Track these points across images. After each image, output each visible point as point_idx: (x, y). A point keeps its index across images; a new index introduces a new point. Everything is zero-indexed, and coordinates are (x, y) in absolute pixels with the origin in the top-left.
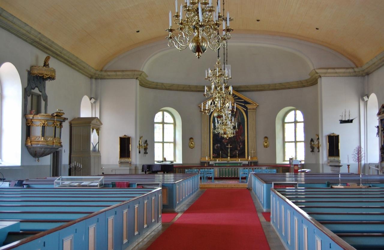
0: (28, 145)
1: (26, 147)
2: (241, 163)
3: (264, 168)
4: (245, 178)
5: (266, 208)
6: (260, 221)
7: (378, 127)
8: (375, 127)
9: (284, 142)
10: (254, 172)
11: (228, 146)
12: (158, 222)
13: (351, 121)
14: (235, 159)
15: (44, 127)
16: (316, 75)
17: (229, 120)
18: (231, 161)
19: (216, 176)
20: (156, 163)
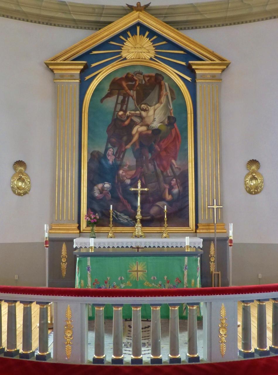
11: (137, 187)
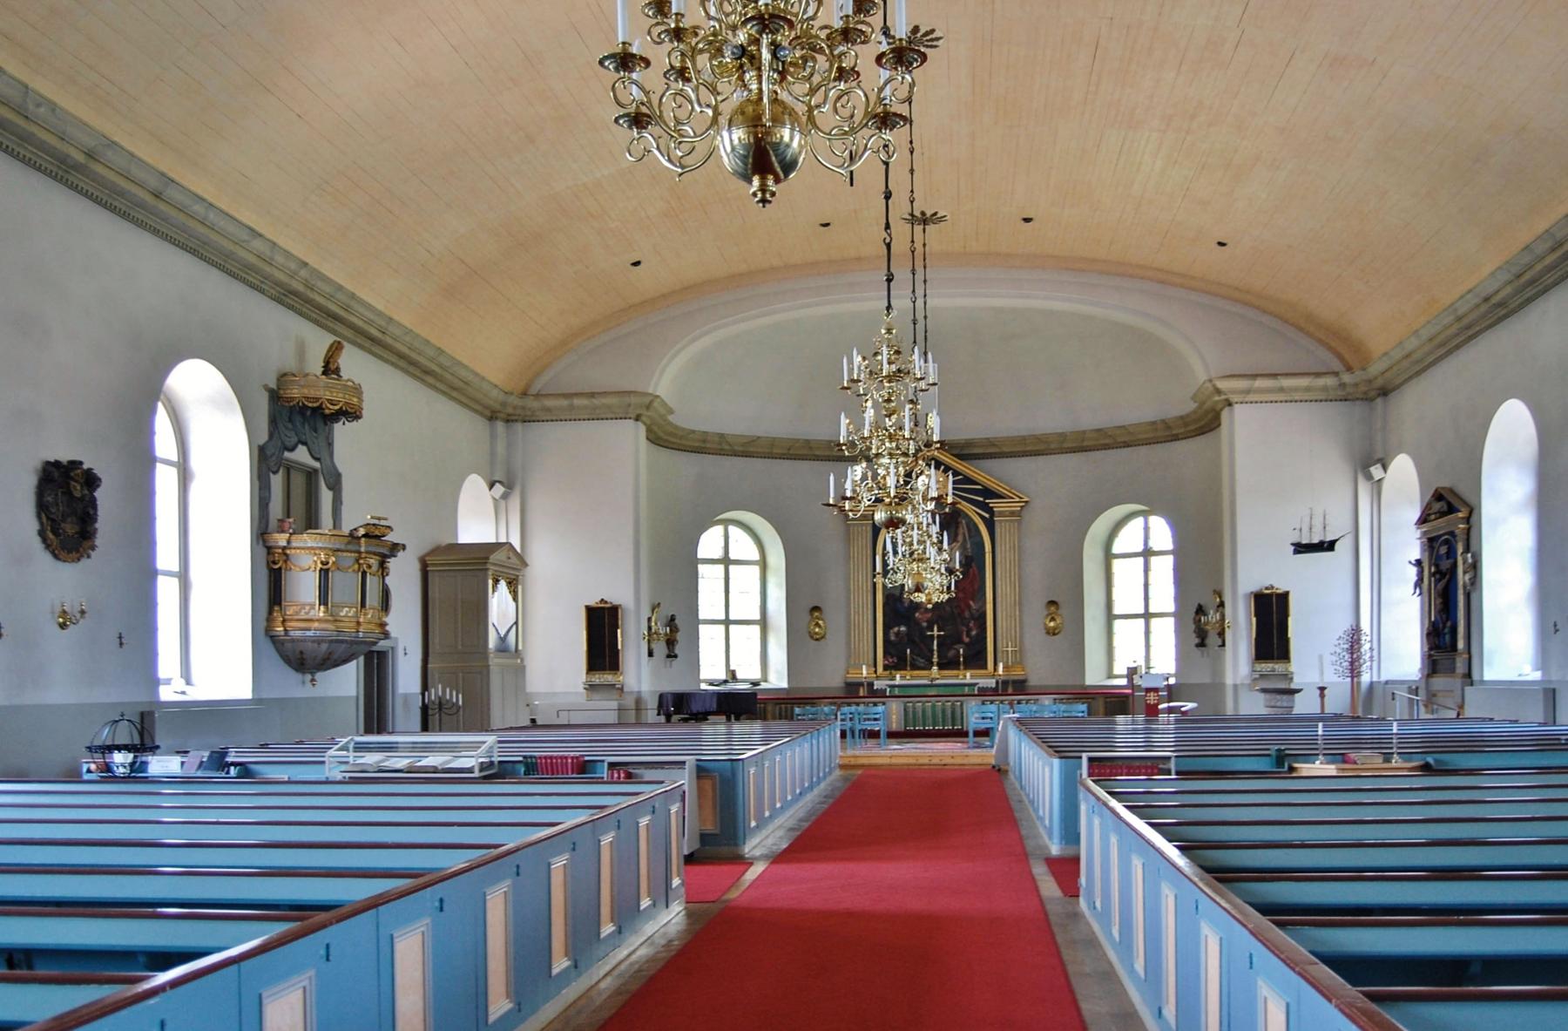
0: (274, 633)
1: (268, 639)
2: (975, 684)
3: (1047, 700)
4: (986, 733)
5: (1061, 843)
6: (1039, 896)
7: (1418, 563)
8: (1410, 562)
9: (1110, 617)
10: (1016, 715)
11: (933, 631)
12: (667, 907)
13: (1329, 546)
14: (955, 672)
15: (324, 573)
16: (1217, 398)
17: (933, 544)
18: (943, 677)
19: (894, 727)
20: (704, 686)
